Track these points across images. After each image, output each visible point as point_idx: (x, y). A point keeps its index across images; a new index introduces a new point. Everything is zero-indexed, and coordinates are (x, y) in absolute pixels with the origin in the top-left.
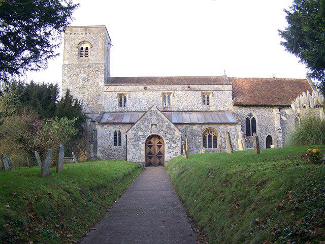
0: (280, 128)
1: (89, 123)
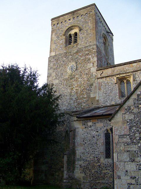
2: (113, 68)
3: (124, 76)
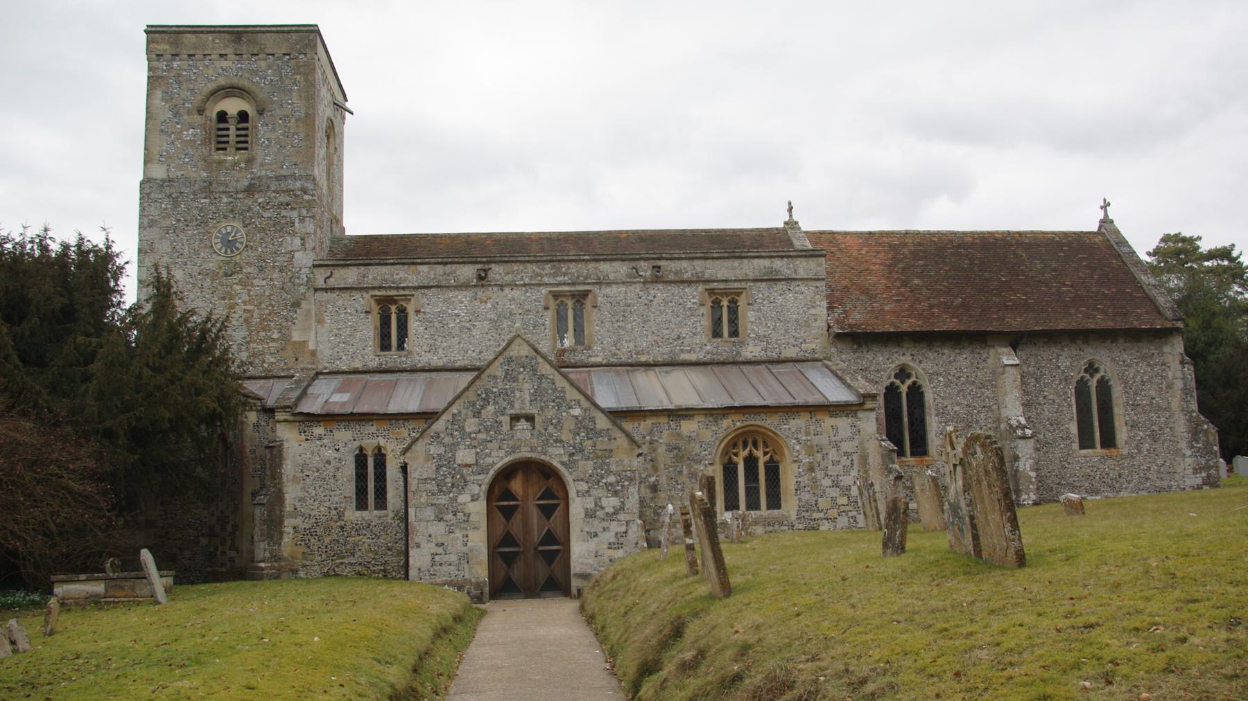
0: (1023, 421)
1: (252, 417)
2: (363, 268)
3: (392, 296)
